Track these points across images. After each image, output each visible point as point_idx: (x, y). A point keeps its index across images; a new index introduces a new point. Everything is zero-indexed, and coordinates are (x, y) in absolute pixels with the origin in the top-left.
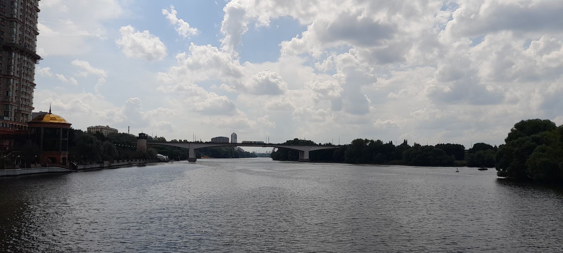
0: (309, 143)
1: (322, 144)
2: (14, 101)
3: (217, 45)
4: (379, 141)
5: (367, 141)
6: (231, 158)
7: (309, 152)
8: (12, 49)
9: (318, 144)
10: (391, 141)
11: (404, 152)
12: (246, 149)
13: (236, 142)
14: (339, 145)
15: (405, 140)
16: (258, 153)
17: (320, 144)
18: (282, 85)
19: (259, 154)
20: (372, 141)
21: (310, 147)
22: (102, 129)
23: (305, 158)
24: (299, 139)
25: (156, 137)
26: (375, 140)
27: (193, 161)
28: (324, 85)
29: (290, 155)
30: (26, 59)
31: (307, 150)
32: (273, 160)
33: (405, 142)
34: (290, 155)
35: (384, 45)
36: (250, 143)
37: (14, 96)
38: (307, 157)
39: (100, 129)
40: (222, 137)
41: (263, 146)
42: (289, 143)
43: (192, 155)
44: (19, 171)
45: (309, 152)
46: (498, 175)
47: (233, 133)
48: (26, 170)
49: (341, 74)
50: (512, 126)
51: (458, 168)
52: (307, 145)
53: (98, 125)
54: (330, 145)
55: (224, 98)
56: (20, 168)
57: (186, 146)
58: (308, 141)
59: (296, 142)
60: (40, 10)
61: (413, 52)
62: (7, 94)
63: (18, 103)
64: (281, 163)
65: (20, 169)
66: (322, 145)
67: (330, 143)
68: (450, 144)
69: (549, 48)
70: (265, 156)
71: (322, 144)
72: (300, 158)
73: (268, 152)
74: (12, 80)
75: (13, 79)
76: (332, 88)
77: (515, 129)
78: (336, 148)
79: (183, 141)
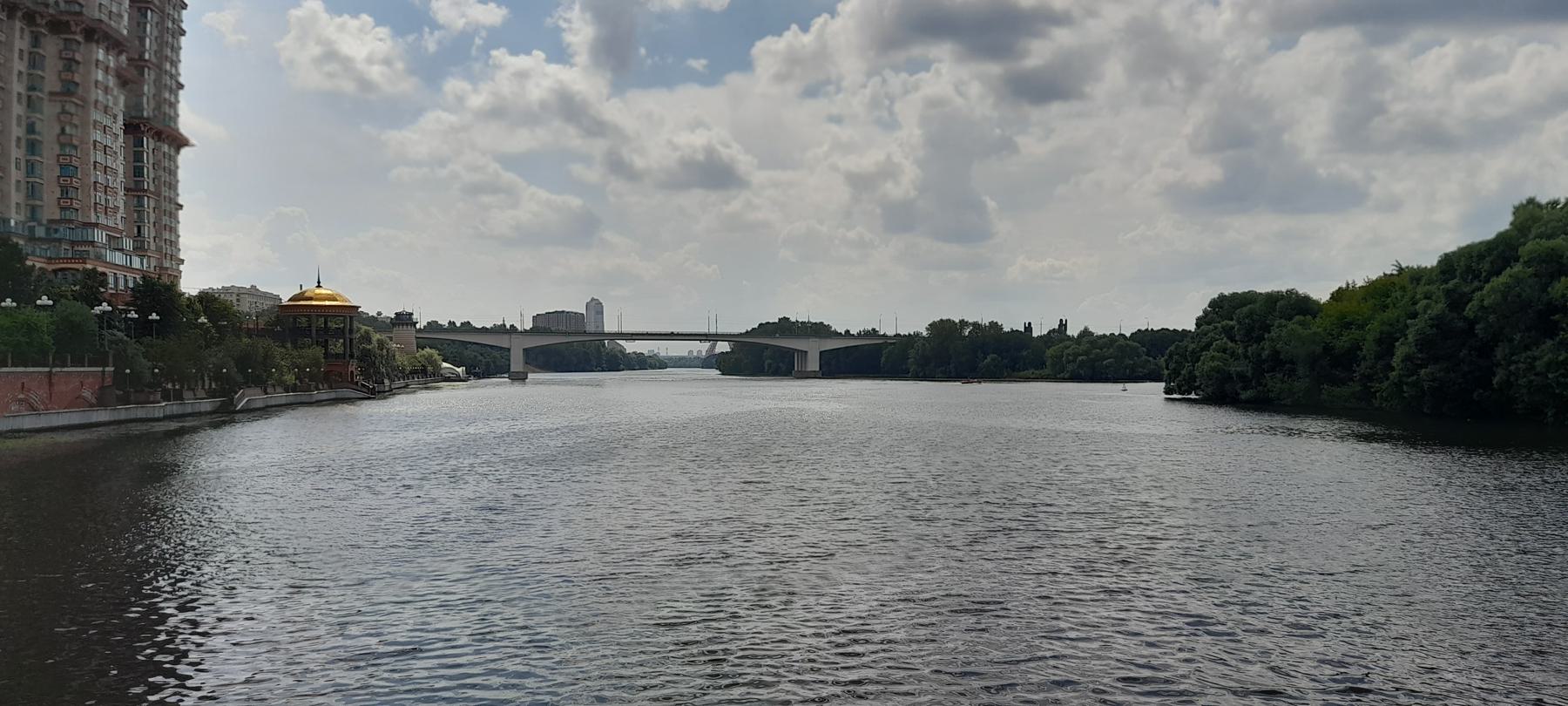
0: (819, 330)
1: (852, 333)
2: (153, 247)
3: (559, 54)
4: (994, 325)
5: (963, 323)
6: (599, 371)
7: (821, 352)
8: (142, 129)
9: (843, 333)
10: (1030, 324)
11: (1049, 352)
12: (630, 347)
13: (600, 329)
14: (898, 335)
15: (1061, 320)
16: (665, 355)
17: (847, 332)
18: (743, 161)
19: (671, 358)
20: (976, 325)
21: (823, 340)
22: (242, 296)
23: (809, 369)
24: (793, 319)
25: (379, 314)
26: (986, 321)
27: (520, 378)
28: (868, 161)
29: (770, 361)
30: (166, 150)
31: (813, 349)
32: (723, 374)
33: (1063, 325)
34: (770, 361)
35: (1038, 53)
36: (167, 235)
37: (152, 235)
38: (813, 365)
39: (234, 296)
40: (563, 312)
41: (700, 340)
42: (764, 329)
43: (517, 364)
44: (161, 408)
45: (821, 352)
46: (1166, 393)
47: (593, 299)
48: (69, 414)
49: (912, 132)
50: (1205, 305)
51: (1126, 384)
52: (816, 337)
53: (228, 285)
54: (873, 333)
55: (576, 202)
56: (164, 401)
57: (502, 341)
58: (816, 323)
59: (785, 327)
60: (185, 32)
61: (1114, 73)
62: (139, 231)
63: (159, 249)
64: (755, 380)
65: (163, 404)
66: (853, 335)
67: (874, 330)
68: (1167, 329)
69: (1471, 68)
70: (687, 363)
71: (854, 332)
72: (796, 369)
73: (695, 354)
74: (146, 198)
75: (148, 197)
76: (888, 171)
77: (1209, 309)
78: (889, 341)
79: (458, 325)
